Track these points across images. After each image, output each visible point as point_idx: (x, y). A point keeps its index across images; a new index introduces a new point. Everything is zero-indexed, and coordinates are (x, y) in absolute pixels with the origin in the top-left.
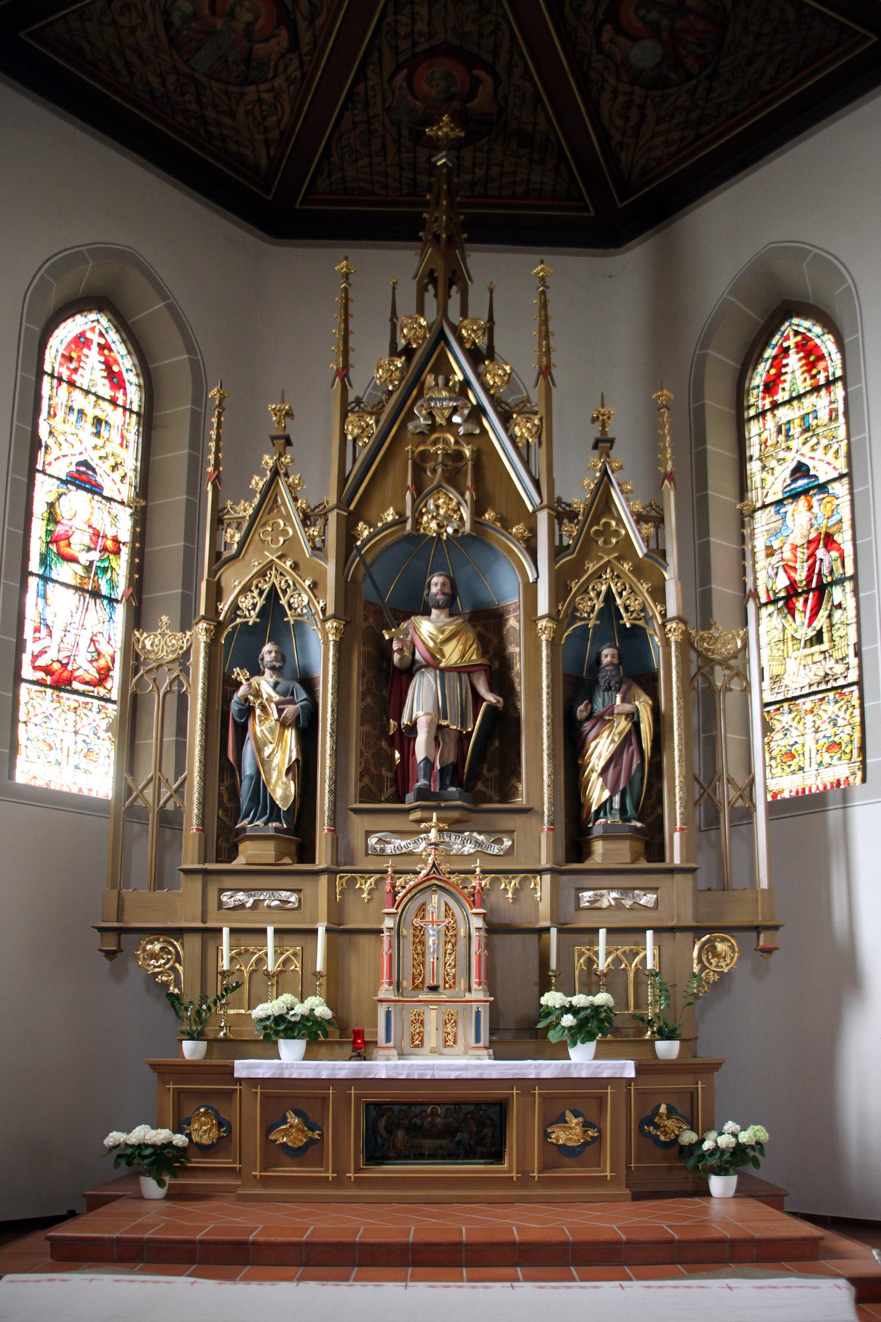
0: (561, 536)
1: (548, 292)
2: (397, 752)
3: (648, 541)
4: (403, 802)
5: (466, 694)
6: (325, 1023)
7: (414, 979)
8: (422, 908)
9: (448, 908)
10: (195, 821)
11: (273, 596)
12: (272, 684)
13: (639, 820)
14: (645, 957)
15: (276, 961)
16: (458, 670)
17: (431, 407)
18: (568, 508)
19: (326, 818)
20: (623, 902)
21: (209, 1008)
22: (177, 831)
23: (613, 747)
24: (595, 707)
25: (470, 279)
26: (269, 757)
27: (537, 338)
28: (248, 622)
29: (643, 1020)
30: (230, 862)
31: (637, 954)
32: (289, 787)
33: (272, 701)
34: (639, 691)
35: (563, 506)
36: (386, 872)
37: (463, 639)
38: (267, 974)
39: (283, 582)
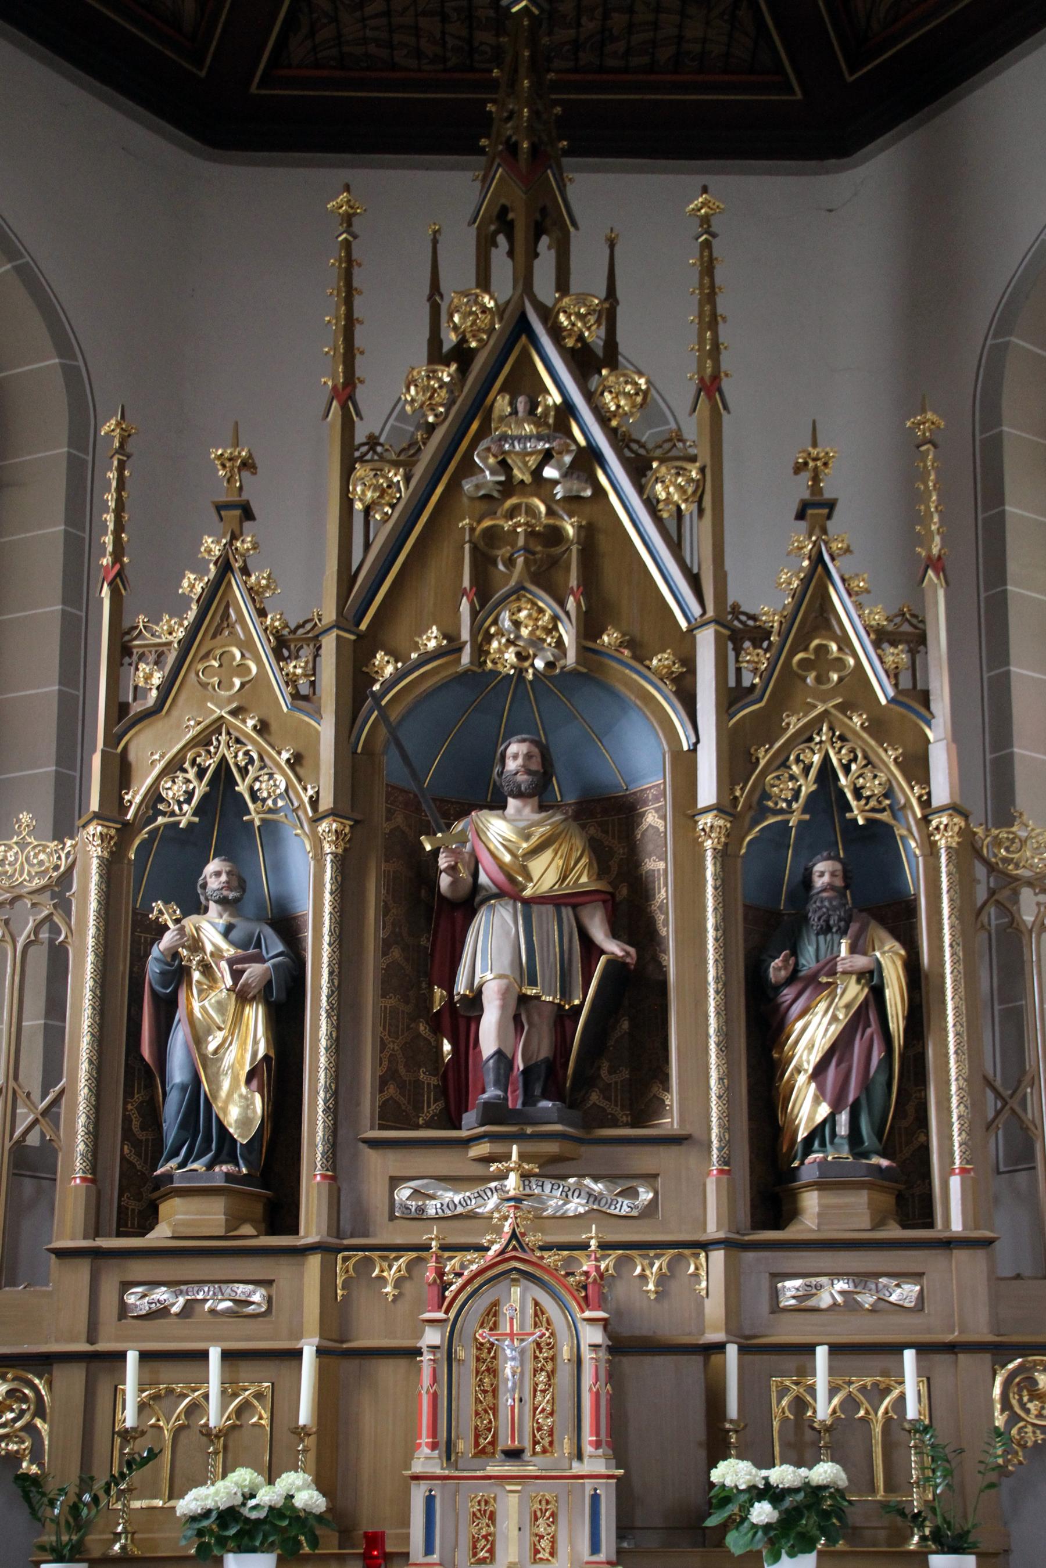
0: (739, 670)
1: (715, 243)
2: (445, 1041)
3: (896, 676)
4: (458, 1127)
5: (570, 941)
6: (312, 1522)
7: (477, 1436)
8: (493, 1311)
9: (539, 1310)
10: (78, 1164)
11: (223, 776)
12: (221, 929)
13: (884, 1156)
14: (902, 1397)
15: (224, 1407)
16: (555, 901)
17: (504, 452)
18: (751, 623)
19: (319, 1156)
20: (859, 1298)
21: (96, 1499)
22: (45, 1183)
23: (835, 1030)
24: (802, 961)
25: (574, 224)
26: (216, 1052)
27: (696, 326)
28: (179, 822)
29: (902, 1513)
30: (143, 1235)
31: (888, 1391)
32: (253, 1103)
33: (222, 957)
34: (882, 934)
35: (743, 618)
36: (428, 1248)
37: (564, 848)
38: (206, 1432)
39: (240, 754)
